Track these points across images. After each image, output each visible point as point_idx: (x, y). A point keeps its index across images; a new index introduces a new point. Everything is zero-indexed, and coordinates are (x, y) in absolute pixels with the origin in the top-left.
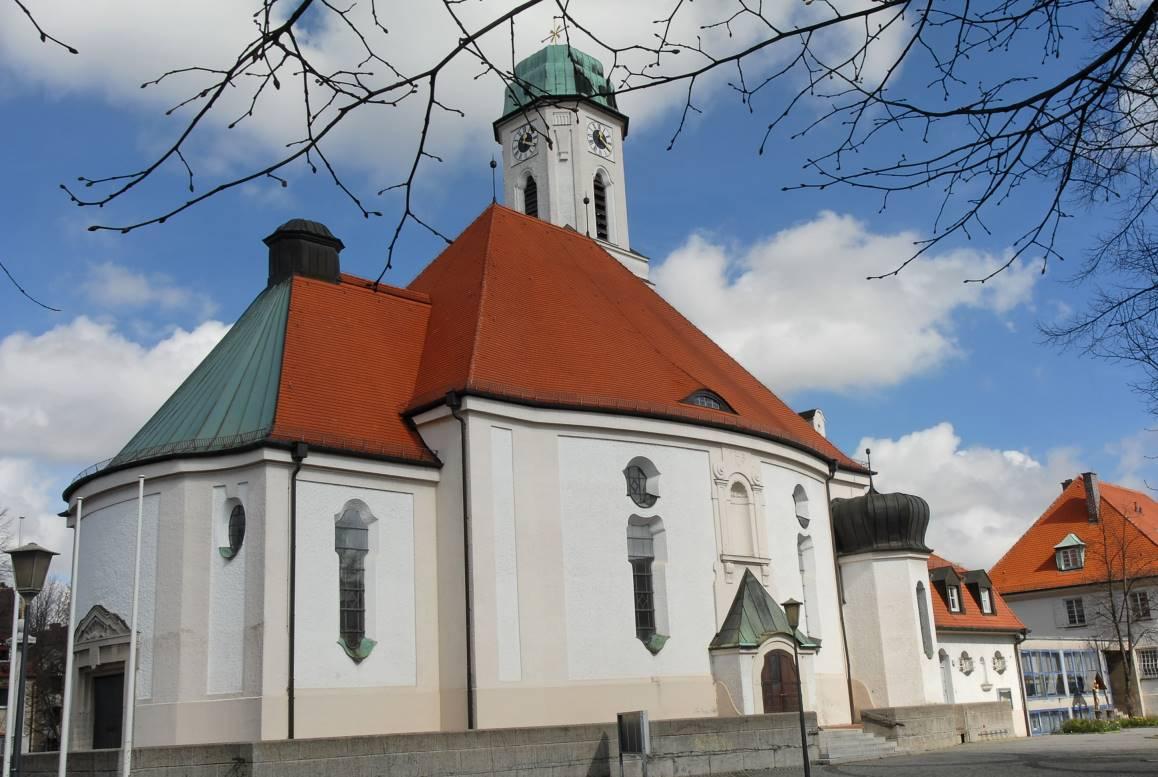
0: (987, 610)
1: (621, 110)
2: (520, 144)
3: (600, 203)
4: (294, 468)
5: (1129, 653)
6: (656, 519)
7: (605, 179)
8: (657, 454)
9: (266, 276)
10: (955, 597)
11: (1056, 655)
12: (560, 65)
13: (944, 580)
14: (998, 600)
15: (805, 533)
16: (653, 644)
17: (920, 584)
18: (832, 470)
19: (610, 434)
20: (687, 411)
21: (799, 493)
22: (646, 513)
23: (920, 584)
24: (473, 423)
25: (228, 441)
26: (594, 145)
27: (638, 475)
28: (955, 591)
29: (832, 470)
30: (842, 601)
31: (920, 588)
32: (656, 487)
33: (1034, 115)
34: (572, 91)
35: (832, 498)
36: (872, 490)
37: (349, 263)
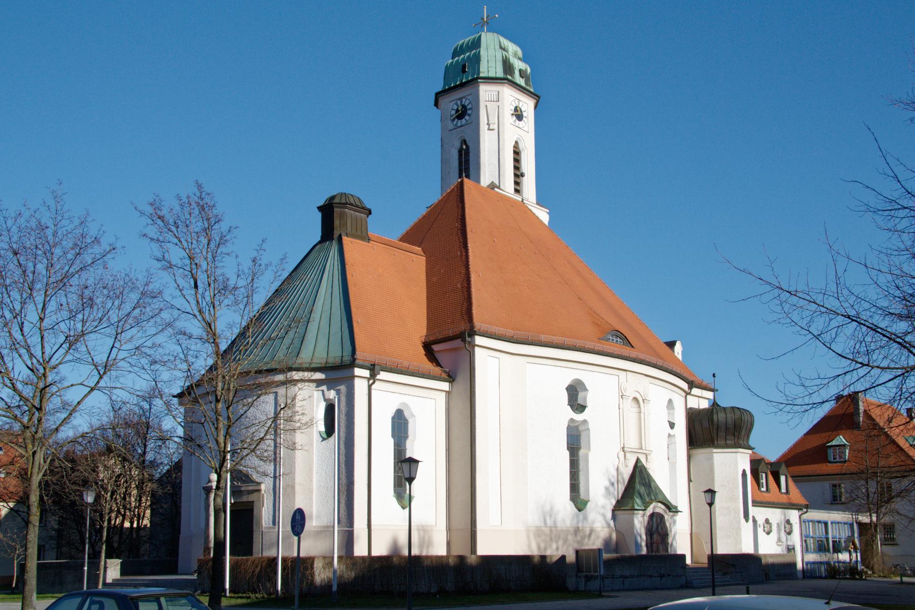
0: (784, 490)
3: (517, 165)
5: (876, 525)
6: (585, 421)
7: (521, 146)
8: (588, 377)
9: (320, 234)
10: (764, 481)
11: (826, 524)
13: (757, 465)
14: (790, 480)
15: (672, 432)
16: (578, 505)
17: (744, 471)
18: (690, 388)
20: (606, 347)
22: (579, 417)
23: (744, 471)
24: (478, 352)
27: (575, 396)
28: (764, 475)
29: (690, 388)
30: (690, 480)
31: (744, 474)
32: (585, 399)
34: (500, 74)
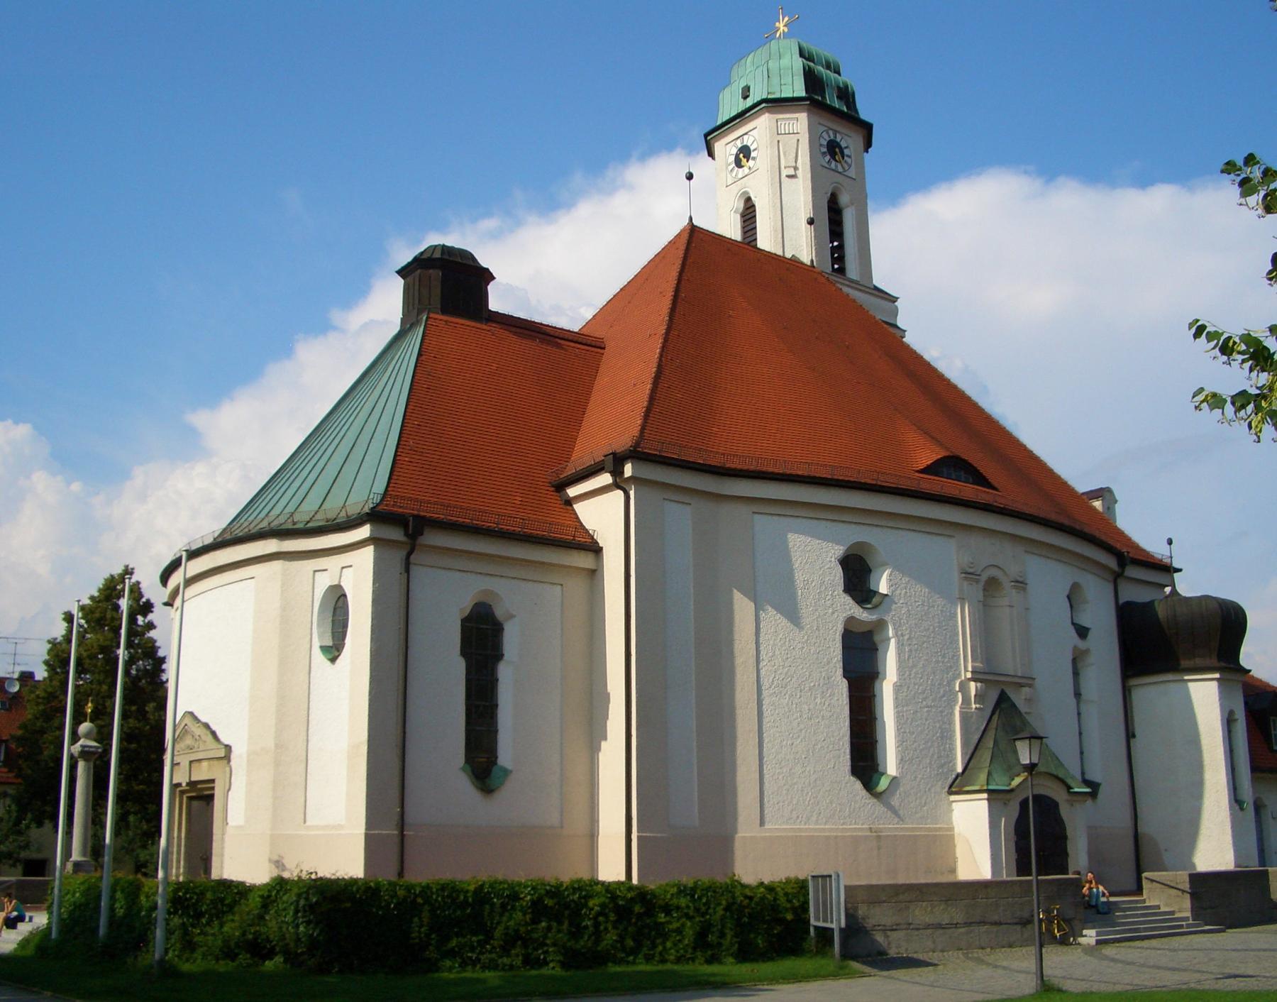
1: (864, 115)
2: (747, 157)
4: (408, 548)
7: (844, 199)
12: (785, 61)
15: (1082, 645)
19: (1027, 524)
21: (1074, 597)
23: (1231, 713)
25: (331, 515)
26: (828, 157)
33: (787, 94)
34: (801, 92)
35: (1121, 602)
36: (1174, 592)
37: (497, 302)
